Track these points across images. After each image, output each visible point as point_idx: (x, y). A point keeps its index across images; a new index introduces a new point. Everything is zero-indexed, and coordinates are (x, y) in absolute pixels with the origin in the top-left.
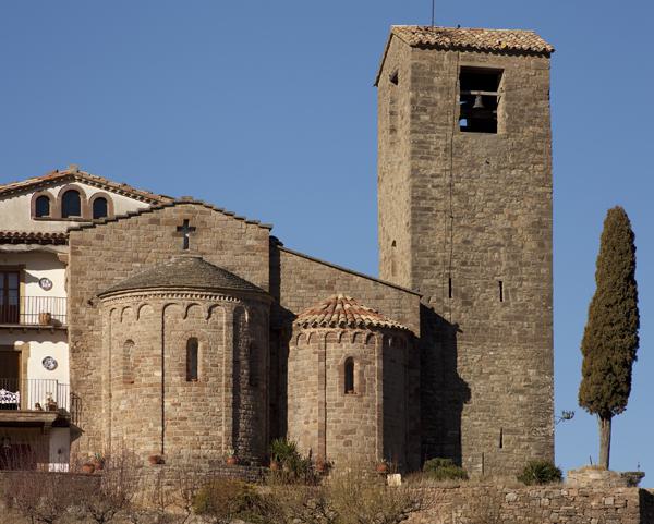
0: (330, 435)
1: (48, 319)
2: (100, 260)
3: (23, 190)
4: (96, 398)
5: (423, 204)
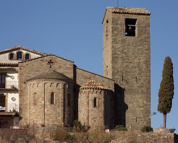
0: (90, 119)
1: (13, 87)
2: (27, 71)
3: (6, 52)
4: (26, 109)
5: (115, 56)
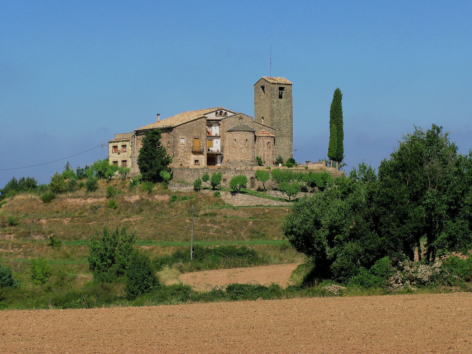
1: (216, 135)
2: (227, 124)
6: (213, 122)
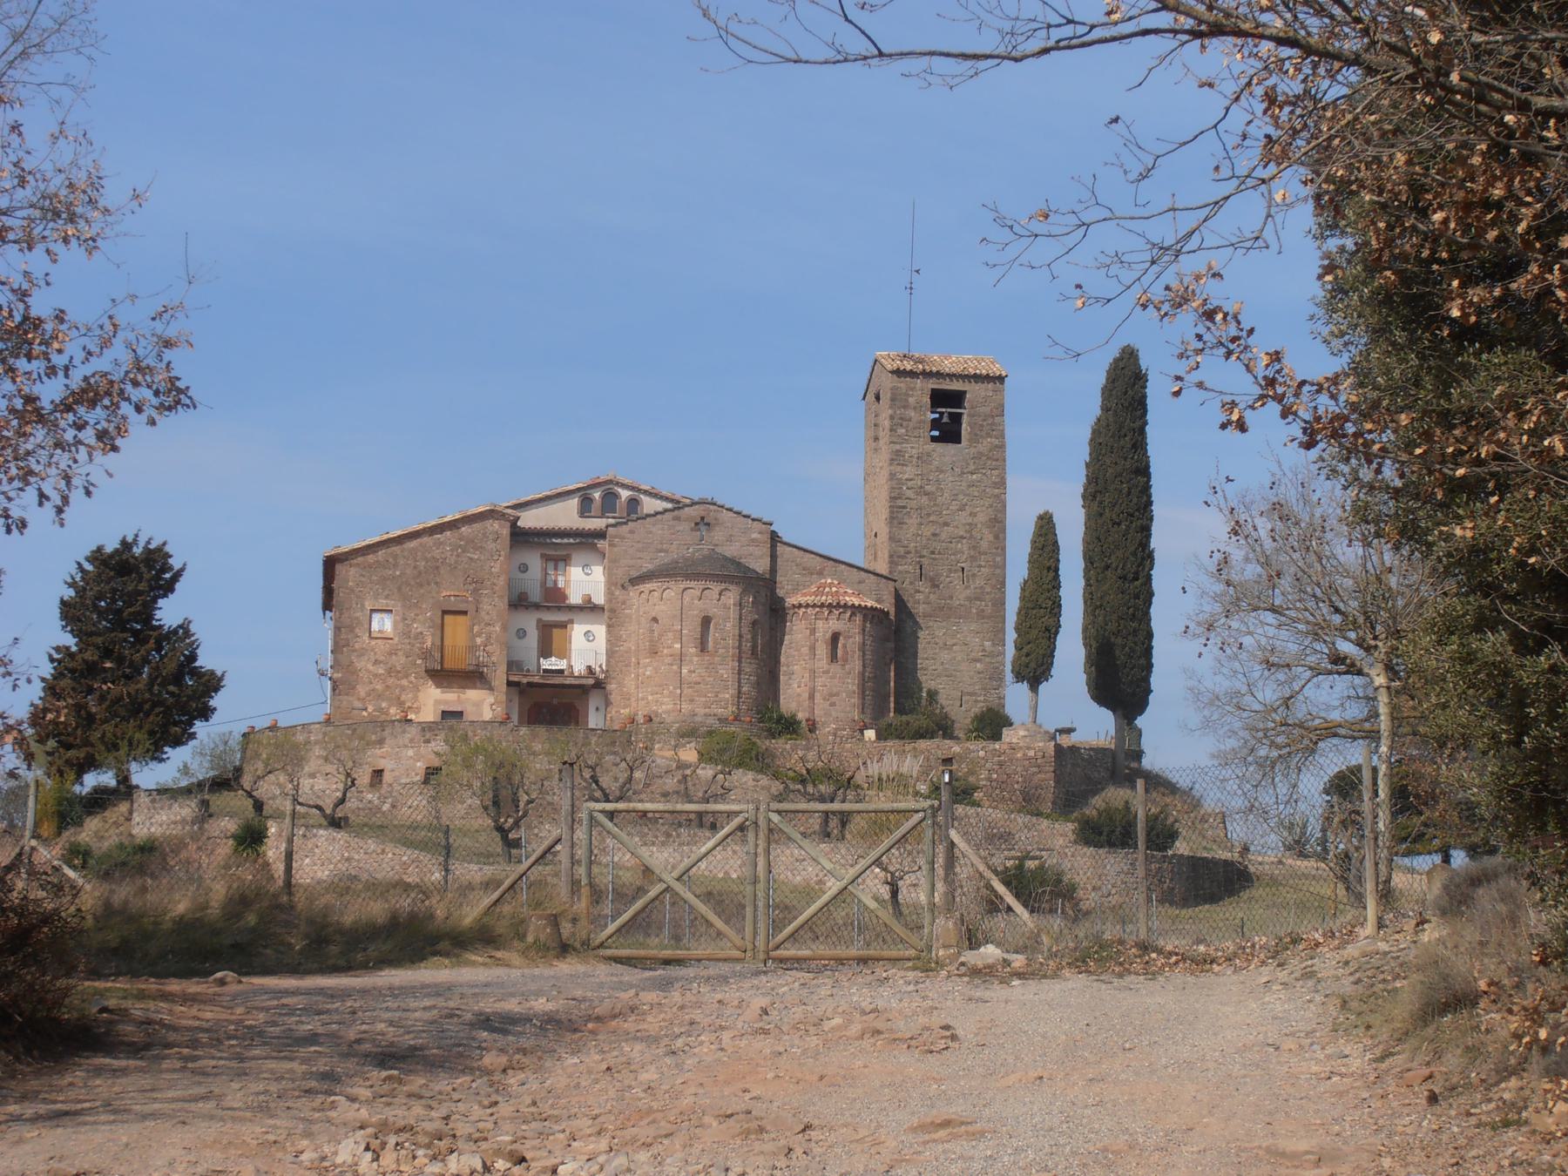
0: (817, 695)
1: (588, 599)
6: (566, 541)
